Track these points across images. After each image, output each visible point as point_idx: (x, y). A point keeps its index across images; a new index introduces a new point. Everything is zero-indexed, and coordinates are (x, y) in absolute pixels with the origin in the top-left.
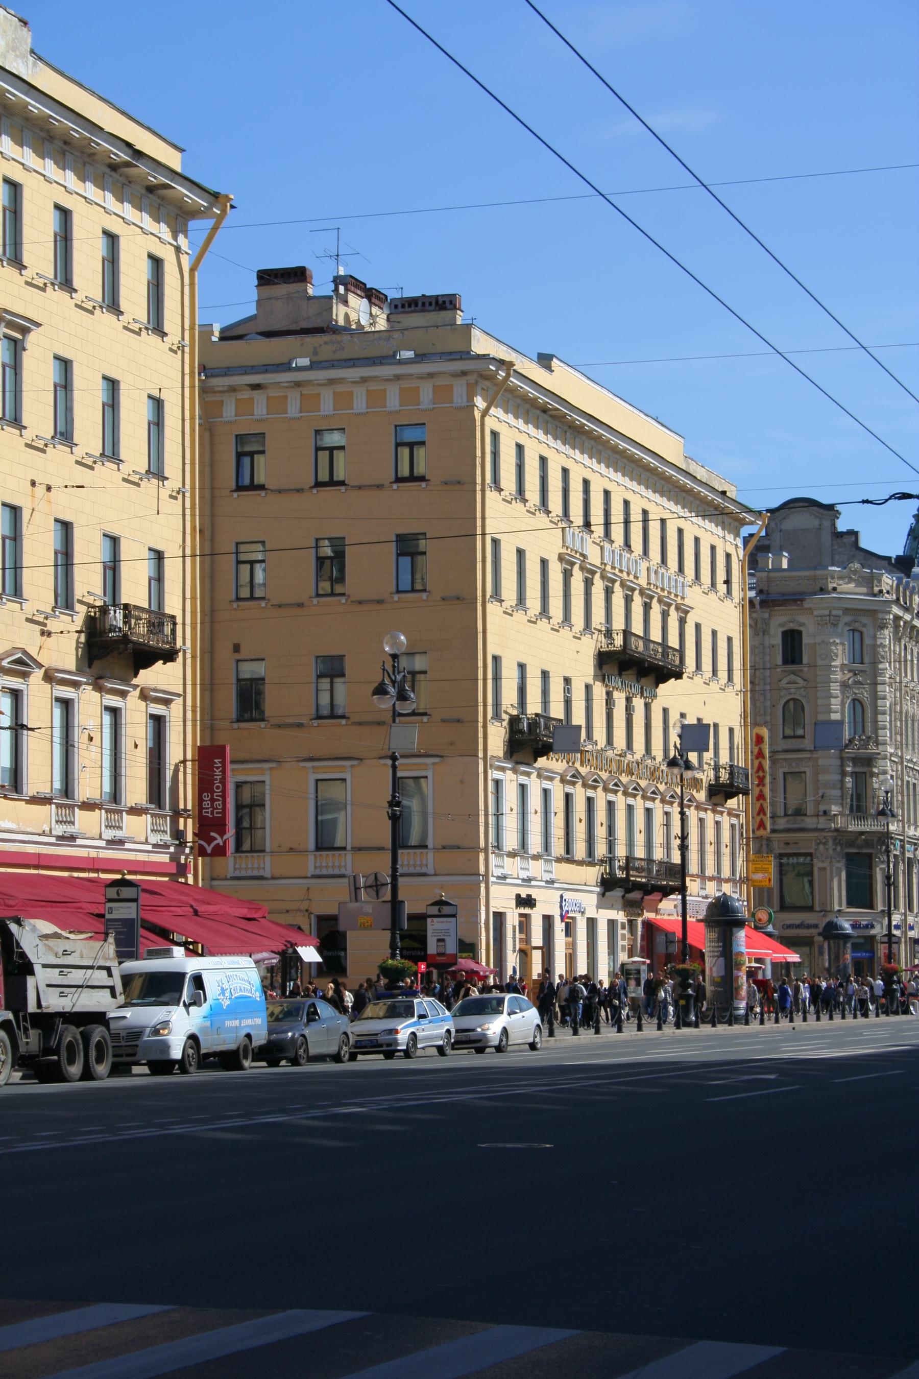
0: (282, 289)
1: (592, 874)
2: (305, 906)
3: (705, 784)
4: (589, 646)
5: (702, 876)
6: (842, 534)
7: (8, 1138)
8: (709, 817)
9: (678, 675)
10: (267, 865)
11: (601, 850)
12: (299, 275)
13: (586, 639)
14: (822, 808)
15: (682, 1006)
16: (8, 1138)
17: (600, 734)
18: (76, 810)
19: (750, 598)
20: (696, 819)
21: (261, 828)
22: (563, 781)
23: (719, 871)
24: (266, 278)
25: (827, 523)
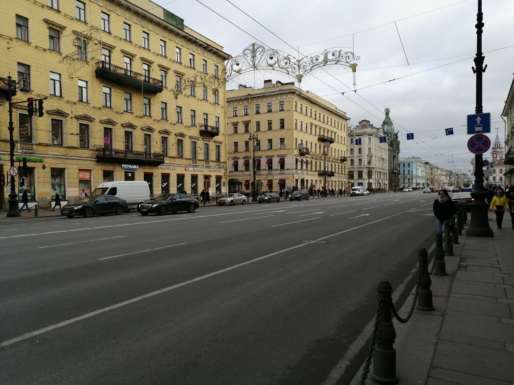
0: (267, 84)
1: (317, 173)
2: (266, 179)
3: (340, 159)
4: (316, 138)
5: (338, 173)
6: (370, 125)
7: (117, 226)
8: (340, 165)
9: (333, 143)
10: (285, 172)
11: (318, 169)
12: (270, 81)
13: (315, 137)
14: (364, 164)
15: (290, 197)
16: (117, 226)
17: (314, 150)
18: (198, 161)
19: (83, 40)
20: (334, 165)
21: (223, 162)
22: (310, 158)
23: (345, 173)
24: (266, 82)
25: (368, 123)
